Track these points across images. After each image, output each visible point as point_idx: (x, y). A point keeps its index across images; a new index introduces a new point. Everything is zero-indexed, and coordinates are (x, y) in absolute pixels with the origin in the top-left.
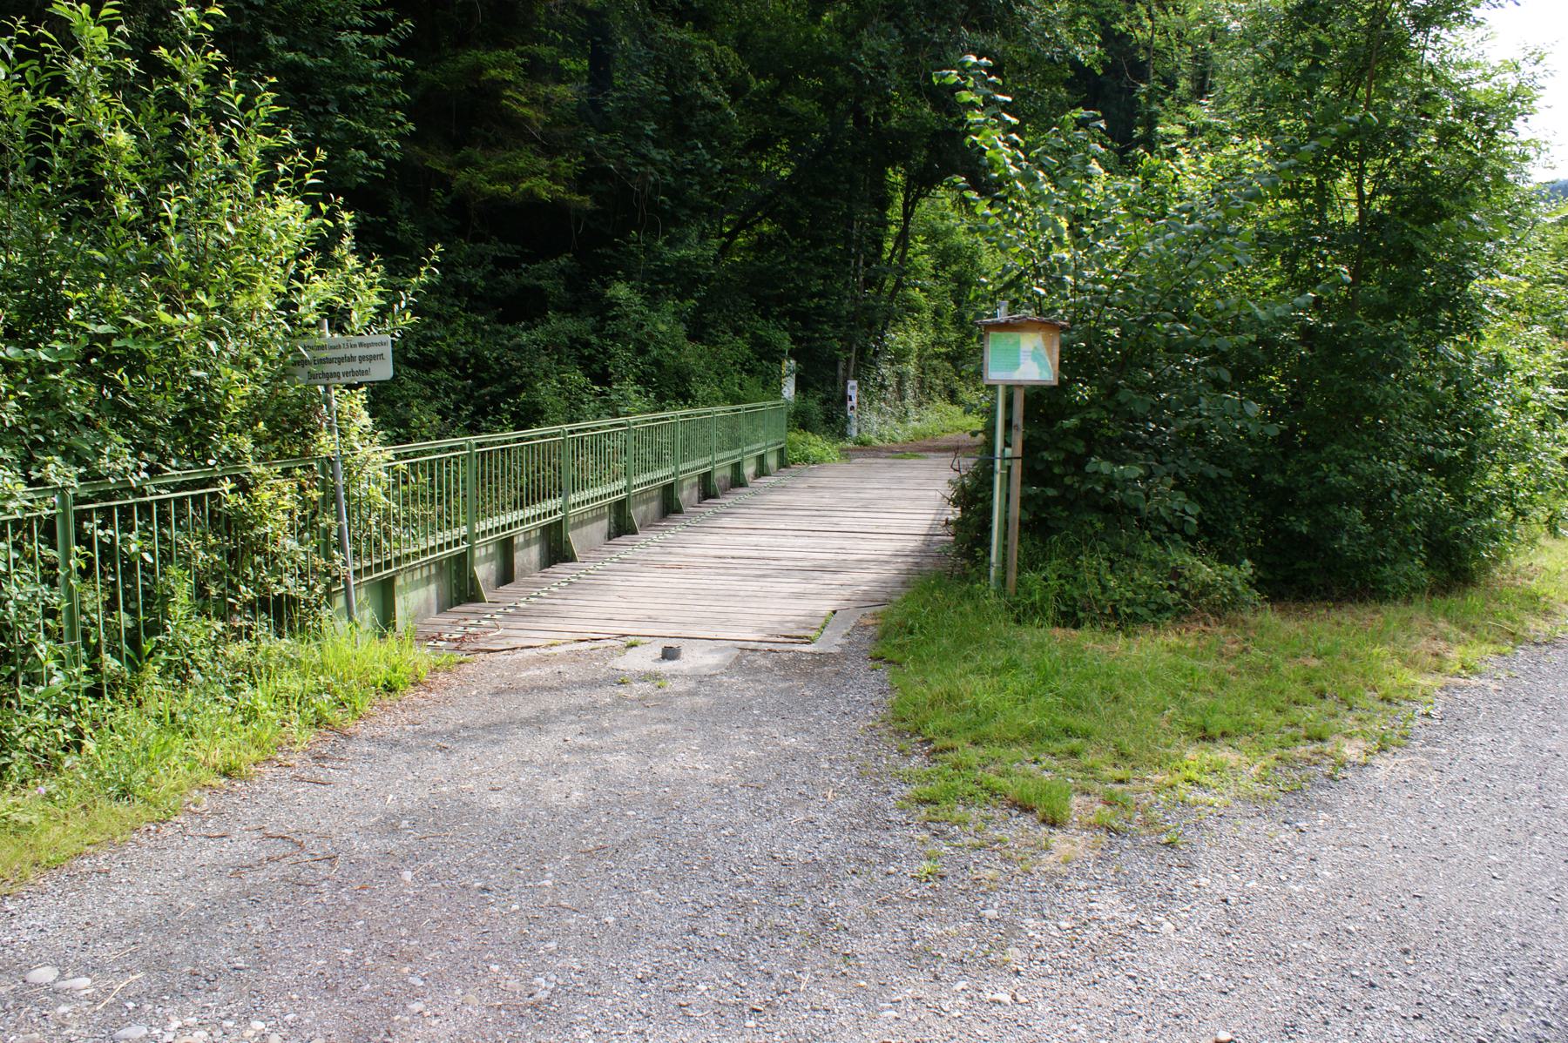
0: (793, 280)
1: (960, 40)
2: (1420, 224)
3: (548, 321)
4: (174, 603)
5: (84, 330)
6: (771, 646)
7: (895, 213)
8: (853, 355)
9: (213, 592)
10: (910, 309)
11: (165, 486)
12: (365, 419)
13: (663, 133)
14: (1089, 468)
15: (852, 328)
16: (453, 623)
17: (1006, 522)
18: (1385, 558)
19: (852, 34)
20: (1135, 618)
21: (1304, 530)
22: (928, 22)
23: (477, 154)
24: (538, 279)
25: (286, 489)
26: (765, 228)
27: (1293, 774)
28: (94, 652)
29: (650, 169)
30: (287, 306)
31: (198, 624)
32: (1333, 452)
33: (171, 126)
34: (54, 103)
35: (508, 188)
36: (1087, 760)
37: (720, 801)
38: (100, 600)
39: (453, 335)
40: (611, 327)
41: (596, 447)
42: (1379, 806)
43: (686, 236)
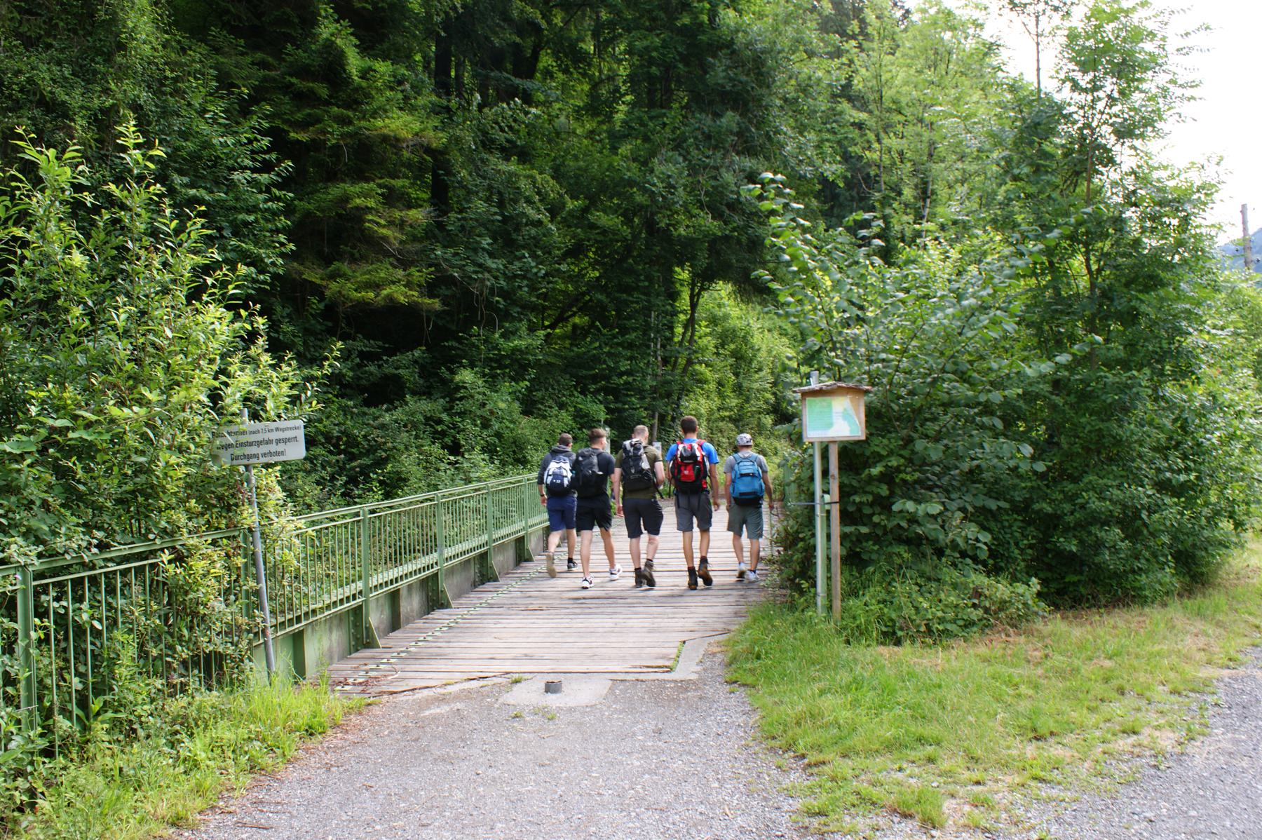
0: (605, 362)
1: (732, 162)
2: (1140, 291)
3: (406, 404)
4: (121, 666)
5: (43, 424)
6: (637, 676)
7: (684, 301)
8: (656, 421)
9: (155, 652)
10: (700, 381)
11: (111, 560)
12: (279, 494)
13: (495, 246)
14: (895, 508)
15: (654, 399)
16: (356, 668)
17: (829, 559)
18: (1140, 569)
19: (645, 163)
20: (946, 633)
21: (1074, 549)
22: (706, 151)
23: (345, 267)
24: (397, 369)
25: (216, 558)
26: (577, 320)
27: (1124, 767)
28: (48, 714)
29: (487, 275)
30: (215, 396)
31: (140, 685)
32: (1090, 482)
33: (117, 248)
34: (19, 232)
35: (372, 295)
36: (945, 766)
37: (631, 825)
38: (54, 666)
39: (328, 418)
40: (459, 406)
41: (453, 507)
42: (1209, 794)
43: (517, 330)
